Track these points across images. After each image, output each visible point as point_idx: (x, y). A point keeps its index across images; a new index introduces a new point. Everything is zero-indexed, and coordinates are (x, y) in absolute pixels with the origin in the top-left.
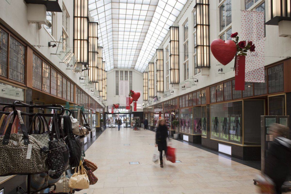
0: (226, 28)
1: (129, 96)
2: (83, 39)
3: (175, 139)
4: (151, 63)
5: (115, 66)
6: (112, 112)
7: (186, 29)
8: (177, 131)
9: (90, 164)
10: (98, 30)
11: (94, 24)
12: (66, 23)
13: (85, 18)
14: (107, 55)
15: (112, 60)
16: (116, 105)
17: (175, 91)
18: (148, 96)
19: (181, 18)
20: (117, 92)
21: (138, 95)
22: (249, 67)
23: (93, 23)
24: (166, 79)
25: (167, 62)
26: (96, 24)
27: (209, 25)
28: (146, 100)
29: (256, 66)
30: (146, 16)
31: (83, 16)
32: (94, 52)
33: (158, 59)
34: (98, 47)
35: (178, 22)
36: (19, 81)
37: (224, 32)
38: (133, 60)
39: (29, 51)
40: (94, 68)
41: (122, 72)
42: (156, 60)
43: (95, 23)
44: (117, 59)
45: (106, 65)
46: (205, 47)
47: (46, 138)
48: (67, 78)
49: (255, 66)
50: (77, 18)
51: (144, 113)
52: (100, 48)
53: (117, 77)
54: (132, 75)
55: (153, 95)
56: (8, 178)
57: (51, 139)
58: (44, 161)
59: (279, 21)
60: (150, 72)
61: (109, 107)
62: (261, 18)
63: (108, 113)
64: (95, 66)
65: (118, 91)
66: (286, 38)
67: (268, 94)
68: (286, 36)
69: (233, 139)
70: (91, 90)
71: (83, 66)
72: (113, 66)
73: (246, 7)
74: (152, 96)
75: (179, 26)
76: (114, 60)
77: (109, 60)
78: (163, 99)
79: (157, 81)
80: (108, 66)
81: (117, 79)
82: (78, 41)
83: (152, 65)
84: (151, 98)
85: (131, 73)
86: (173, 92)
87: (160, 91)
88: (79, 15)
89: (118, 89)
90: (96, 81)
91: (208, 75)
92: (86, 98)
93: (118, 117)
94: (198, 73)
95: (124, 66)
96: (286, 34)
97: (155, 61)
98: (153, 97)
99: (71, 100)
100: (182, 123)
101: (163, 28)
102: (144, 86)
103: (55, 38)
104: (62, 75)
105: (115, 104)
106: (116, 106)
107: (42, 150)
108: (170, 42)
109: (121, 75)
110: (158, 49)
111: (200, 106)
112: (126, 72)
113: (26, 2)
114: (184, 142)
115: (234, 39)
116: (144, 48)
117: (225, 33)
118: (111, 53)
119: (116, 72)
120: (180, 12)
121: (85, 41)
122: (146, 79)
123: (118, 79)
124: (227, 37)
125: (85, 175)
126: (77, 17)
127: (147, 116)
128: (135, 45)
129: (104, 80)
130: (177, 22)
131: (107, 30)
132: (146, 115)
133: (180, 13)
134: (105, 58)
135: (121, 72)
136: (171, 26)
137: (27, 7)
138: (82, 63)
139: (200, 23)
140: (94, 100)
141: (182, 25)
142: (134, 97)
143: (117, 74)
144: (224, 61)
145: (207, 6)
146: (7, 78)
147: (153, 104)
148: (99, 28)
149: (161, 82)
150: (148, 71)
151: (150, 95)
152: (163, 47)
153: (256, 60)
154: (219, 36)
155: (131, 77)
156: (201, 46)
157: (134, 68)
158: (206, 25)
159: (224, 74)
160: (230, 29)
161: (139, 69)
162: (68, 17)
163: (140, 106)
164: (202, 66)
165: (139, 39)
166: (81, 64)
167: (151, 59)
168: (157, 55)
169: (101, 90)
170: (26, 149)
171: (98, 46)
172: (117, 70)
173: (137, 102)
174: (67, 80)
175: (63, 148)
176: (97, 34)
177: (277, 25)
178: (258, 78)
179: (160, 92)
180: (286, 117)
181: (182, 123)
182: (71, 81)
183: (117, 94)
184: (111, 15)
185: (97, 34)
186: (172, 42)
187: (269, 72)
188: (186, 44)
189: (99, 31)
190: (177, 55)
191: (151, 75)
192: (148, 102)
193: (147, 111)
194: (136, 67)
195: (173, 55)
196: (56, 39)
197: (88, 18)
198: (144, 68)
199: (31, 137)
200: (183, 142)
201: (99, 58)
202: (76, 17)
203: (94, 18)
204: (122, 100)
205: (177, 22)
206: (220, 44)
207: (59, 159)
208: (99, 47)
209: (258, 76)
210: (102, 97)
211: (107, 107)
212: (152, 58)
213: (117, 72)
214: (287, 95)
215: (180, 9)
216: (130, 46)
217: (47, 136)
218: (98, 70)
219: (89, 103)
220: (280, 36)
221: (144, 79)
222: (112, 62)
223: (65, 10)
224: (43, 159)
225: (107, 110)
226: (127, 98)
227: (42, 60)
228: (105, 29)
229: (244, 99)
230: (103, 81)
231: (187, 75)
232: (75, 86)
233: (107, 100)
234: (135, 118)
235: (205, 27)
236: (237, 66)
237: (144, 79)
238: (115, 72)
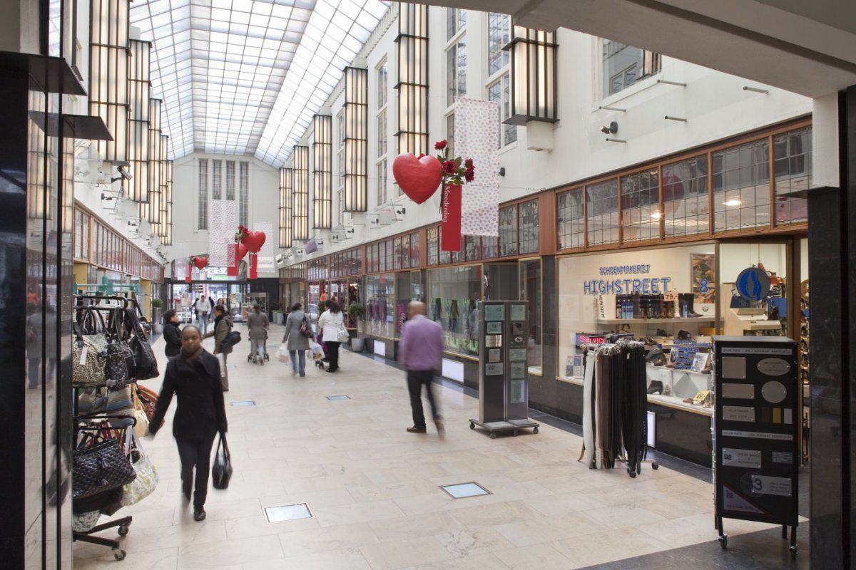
1: (236, 240)
2: (114, 101)
3: (356, 352)
4: (323, 116)
5: (198, 146)
6: (186, 278)
8: (360, 330)
9: (149, 394)
10: (151, 64)
13: (119, 50)
14: (174, 116)
15: (187, 126)
16: (199, 258)
17: (357, 229)
18: (311, 226)
19: (373, 48)
20: (203, 221)
21: (261, 239)
22: (469, 203)
23: (137, 41)
24: (338, 195)
26: (146, 46)
28: (286, 247)
29: (485, 204)
30: (289, 19)
32: (139, 121)
35: (366, 57)
38: (246, 144)
41: (217, 163)
42: (344, 102)
44: (203, 129)
45: (163, 114)
46: (417, 137)
47: (101, 340)
49: (482, 204)
51: (281, 282)
52: (140, 44)
53: (203, 178)
54: (247, 174)
55: (304, 234)
57: (109, 341)
58: (102, 368)
59: (527, 122)
60: (317, 146)
61: (179, 263)
62: (494, 114)
63: (173, 281)
64: (143, 160)
65: (206, 217)
66: (538, 152)
67: (519, 255)
68: (539, 150)
69: (466, 346)
70: (129, 222)
71: (115, 168)
72: (192, 145)
74: (303, 238)
75: (368, 68)
76: (194, 130)
77: (178, 114)
78: (329, 248)
79: (314, 200)
80: (178, 144)
81: (203, 182)
83: (304, 153)
84: (298, 241)
85: (244, 167)
86: (353, 231)
87: (321, 226)
89: (206, 213)
91: (550, 151)
93: (204, 290)
95: (224, 146)
98: (304, 239)
100: (371, 312)
101: (330, 63)
102: (280, 208)
105: (195, 254)
106: (200, 262)
107: (99, 355)
109: (228, 173)
111: (409, 271)
112: (231, 164)
114: (375, 357)
115: (441, 153)
118: (186, 111)
119: (200, 163)
120: (369, 34)
121: (119, 107)
122: (286, 188)
123: (234, 185)
125: (139, 411)
127: (290, 290)
128: (263, 75)
130: (364, 56)
131: (172, 23)
132: (287, 286)
133: (371, 36)
134: (167, 125)
135: (241, 165)
138: (111, 162)
139: (406, 81)
141: (376, 67)
142: (249, 242)
143: (203, 168)
144: (420, 196)
145: (423, 42)
147: (304, 260)
148: (163, 108)
149: (325, 202)
150: (311, 142)
151: (317, 222)
152: (331, 111)
153: (484, 193)
154: (446, 116)
155: (244, 179)
156: (408, 133)
157: (253, 155)
159: (683, 122)
160: (497, 84)
161: (270, 158)
163: (271, 263)
165: (279, 50)
167: (321, 103)
168: (294, 159)
169: (156, 220)
170: (80, 353)
172: (202, 156)
173: (258, 253)
175: (126, 353)
176: (149, 63)
177: (525, 125)
178: (488, 228)
179: (322, 228)
180: (523, 303)
181: (371, 312)
182: (83, 209)
183: (203, 225)
184: (189, 42)
185: (149, 63)
186: (350, 106)
187: (290, 295)
190: (361, 140)
191: (300, 181)
192: (294, 252)
193: (288, 275)
194: (260, 151)
198: (283, 155)
199: (85, 337)
200: (373, 359)
204: (219, 241)
206: (410, 165)
207: (120, 367)
209: (487, 223)
210: (148, 224)
211: (173, 263)
213: (203, 163)
214: (543, 261)
216: (246, 78)
217: (103, 337)
220: (529, 149)
221: (282, 186)
222: (188, 135)
224: (101, 365)
225: (173, 273)
226: (229, 245)
228: (165, 19)
229: (484, 261)
231: (381, 196)
233: (171, 245)
234: (255, 295)
235: (417, 89)
236: (446, 204)
237: (280, 188)
238: (197, 164)
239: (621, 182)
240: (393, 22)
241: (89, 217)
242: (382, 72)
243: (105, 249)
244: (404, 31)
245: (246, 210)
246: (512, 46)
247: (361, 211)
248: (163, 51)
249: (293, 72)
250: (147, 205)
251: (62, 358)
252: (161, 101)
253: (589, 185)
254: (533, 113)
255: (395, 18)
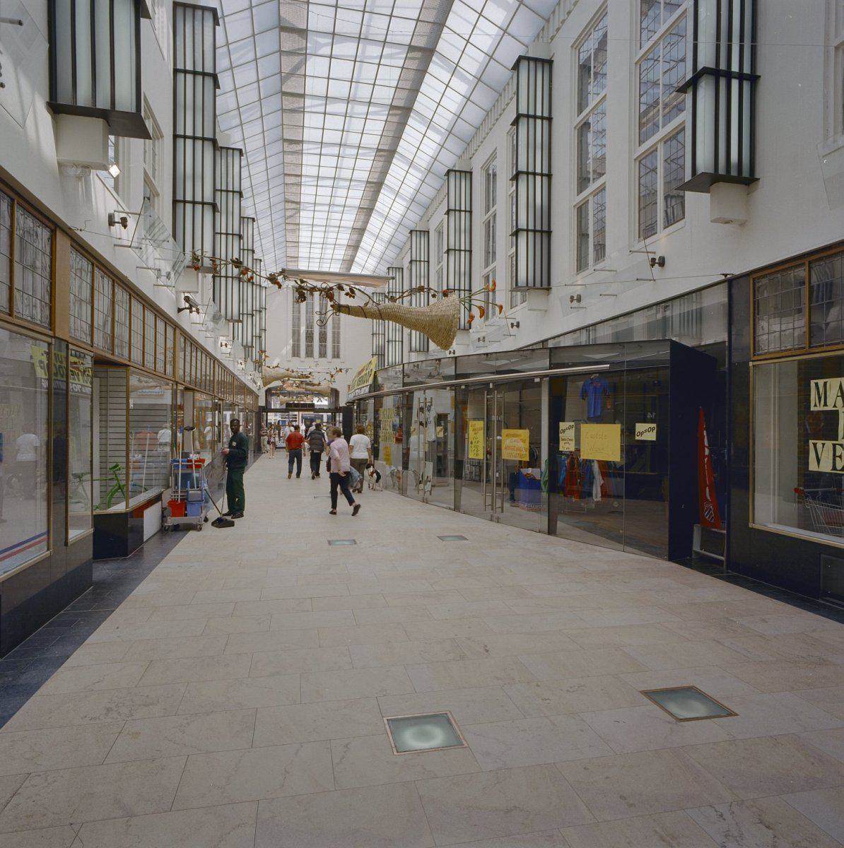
0: (593, 187)
7: (491, 178)
11: (199, 13)
12: (154, 154)
23: (228, 149)
25: (439, 267)
26: (237, 153)
27: (549, 176)
31: (230, 232)
33: (414, 258)
34: (240, 217)
35: (471, 158)
36: (39, 322)
37: (586, 197)
39: (62, 242)
40: (199, 207)
43: (233, 149)
48: (157, 311)
50: (182, 140)
56: (21, 569)
73: (642, 139)
82: (187, 205)
88: (224, 231)
90: (236, 317)
91: (546, 311)
92: (208, 364)
94: (519, 304)
96: (728, 216)
97: (406, 265)
99: (165, 372)
103: (123, 201)
104: (143, 303)
108: (448, 212)
110: (452, 170)
113: (53, 110)
116: (422, 104)
117: (591, 198)
124: (595, 212)
126: (185, 137)
129: (258, 313)
133: (476, 133)
136: (451, 167)
137: (56, 123)
140: (229, 370)
146: (11, 315)
148: (244, 163)
158: (542, 175)
159: (614, 298)
162: (158, 139)
164: (722, 170)
166: (99, 122)
171: (242, 215)
174: (156, 315)
185: (240, 180)
188: (489, 221)
189: (245, 173)
190: (465, 251)
195: (455, 250)
196: (129, 208)
197: (214, 141)
201: (243, 250)
202: (180, 136)
203: (229, 135)
205: (466, 156)
208: (244, 218)
212: (398, 255)
215: (477, 123)
218: (241, 283)
219: (216, 378)
220: (714, 221)
223: (151, 119)
227: (93, 264)
230: (254, 317)
232: (178, 332)
239: (810, 268)
240: (508, 104)
241: (175, 330)
242: (440, 233)
243: (203, 373)
244: (523, 110)
245: (338, 337)
246: (693, 84)
247: (465, 329)
248: (264, 224)
249: (455, 13)
250: (240, 324)
251: (125, 502)
252: (253, 220)
253: (816, 260)
254: (722, 170)
255: (511, 99)
